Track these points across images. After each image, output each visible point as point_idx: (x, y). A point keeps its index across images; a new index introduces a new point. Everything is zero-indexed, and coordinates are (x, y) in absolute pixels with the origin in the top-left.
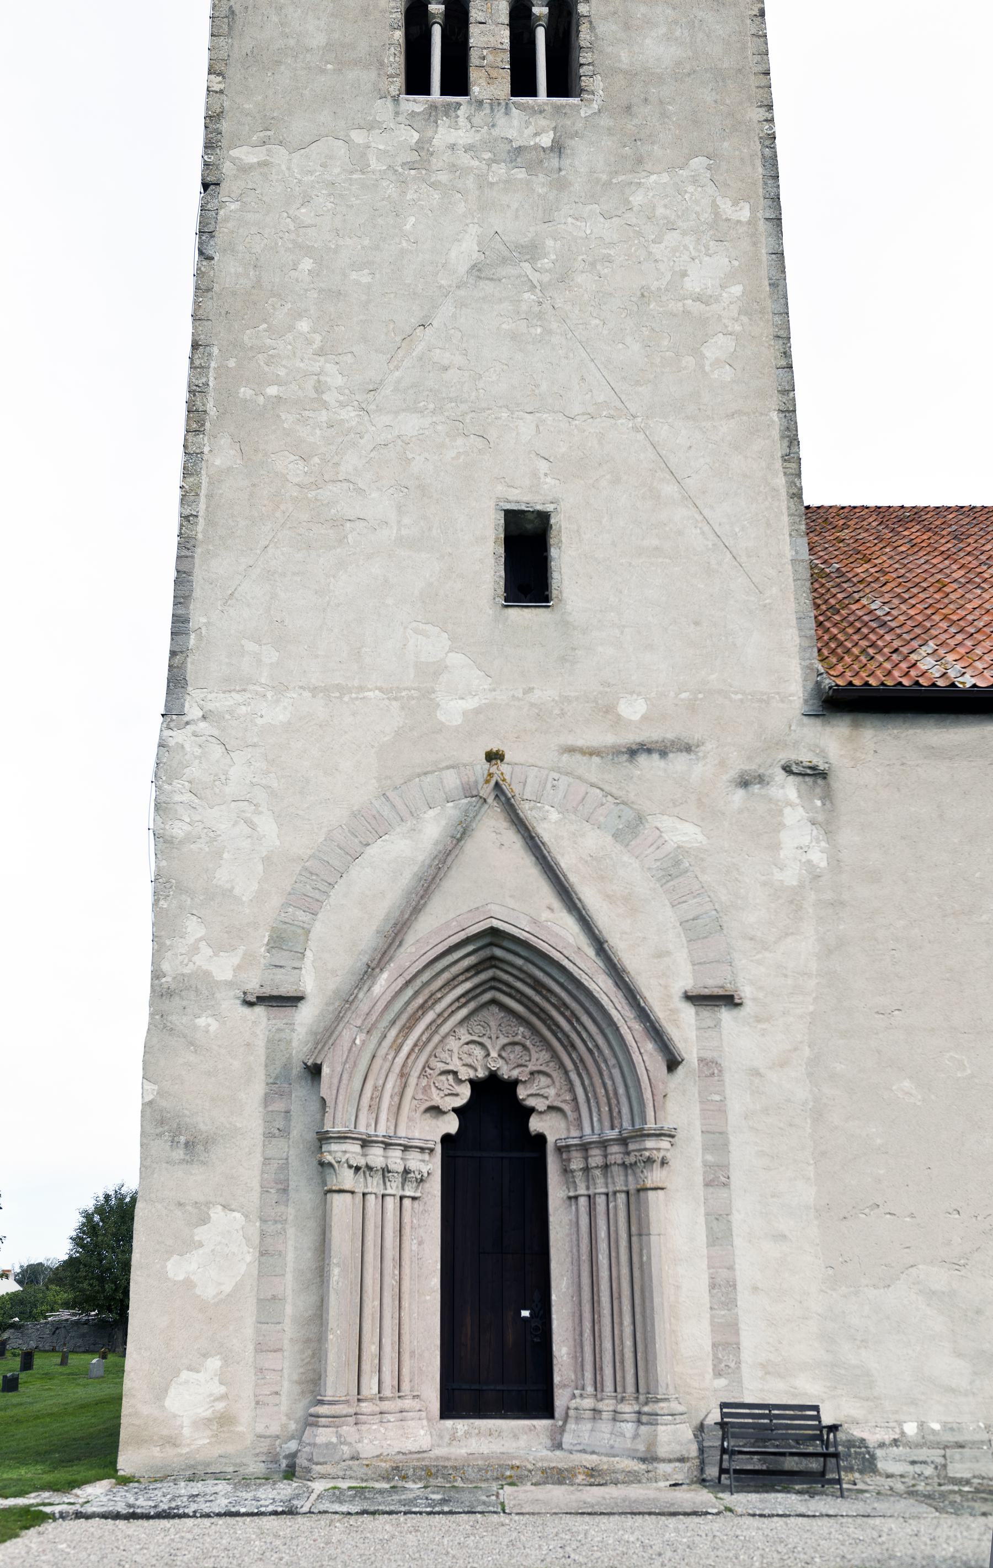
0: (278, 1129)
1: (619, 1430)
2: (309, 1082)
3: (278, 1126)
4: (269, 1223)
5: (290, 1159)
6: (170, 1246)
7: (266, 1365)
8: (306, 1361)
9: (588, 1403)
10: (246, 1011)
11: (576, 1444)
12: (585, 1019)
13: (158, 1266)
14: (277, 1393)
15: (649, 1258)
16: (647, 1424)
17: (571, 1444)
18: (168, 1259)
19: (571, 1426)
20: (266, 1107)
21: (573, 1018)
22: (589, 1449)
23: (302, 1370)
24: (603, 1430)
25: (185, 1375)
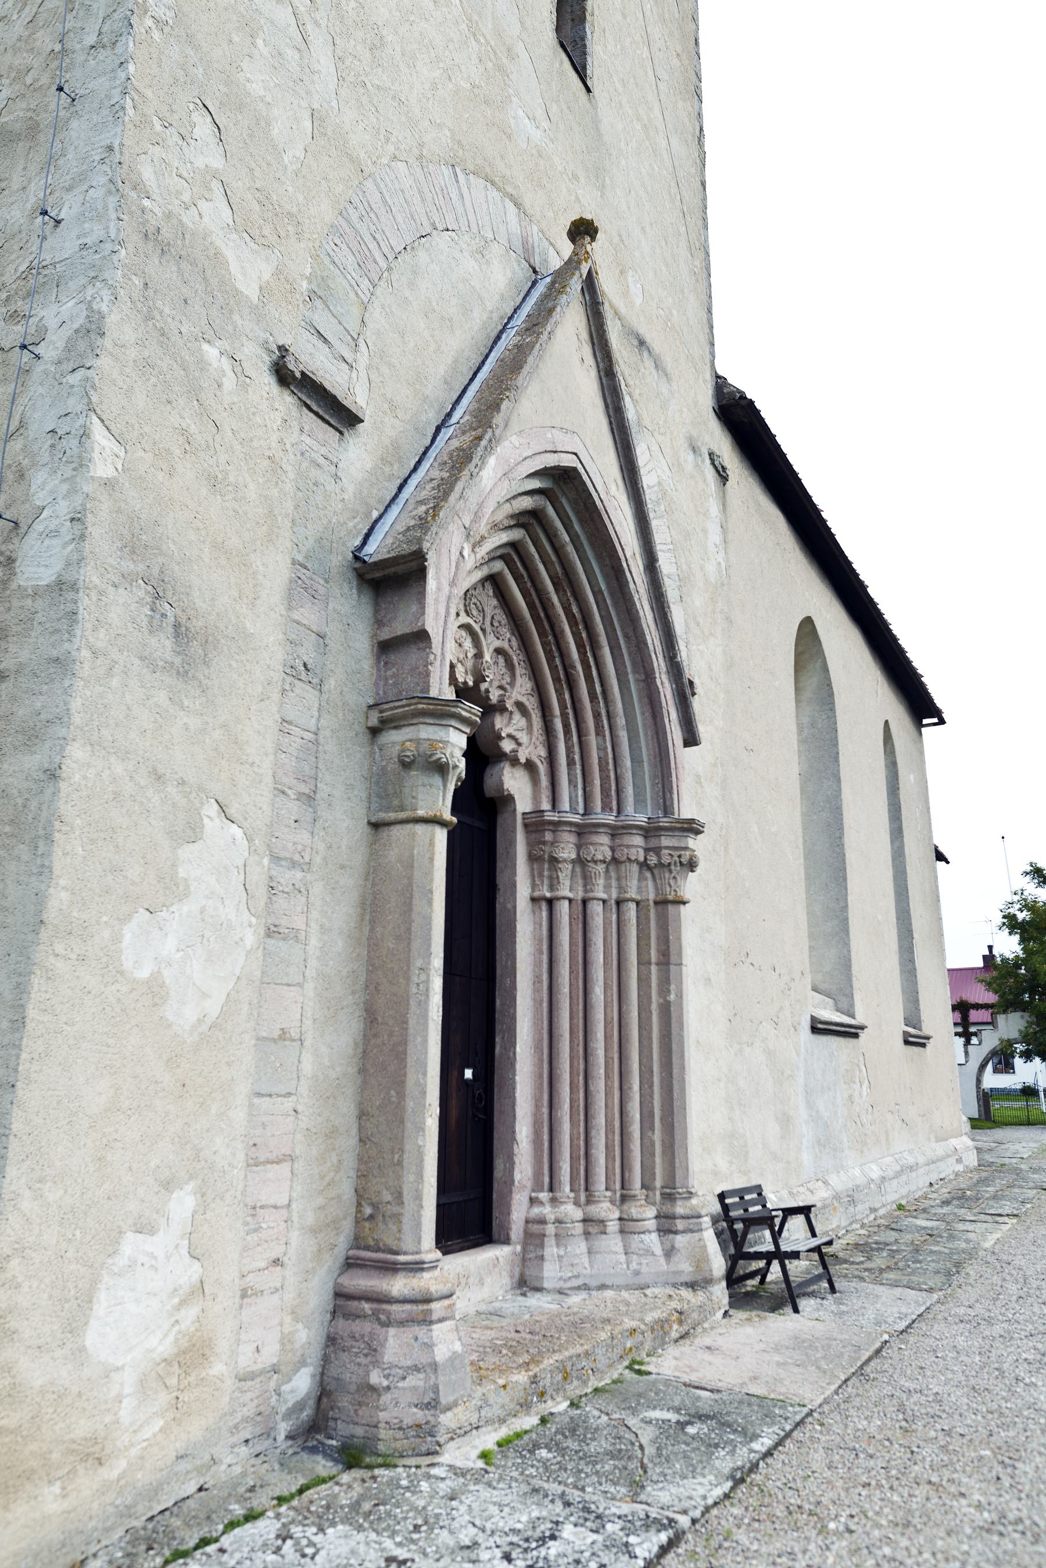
0: (305, 665)
1: (641, 1246)
2: (354, 591)
3: (305, 658)
4: (283, 863)
5: (321, 732)
6: (133, 883)
7: (264, 1199)
8: (327, 1179)
9: (572, 1212)
10: (268, 381)
11: (570, 1278)
12: (606, 652)
13: (106, 934)
14: (277, 1262)
15: (680, 996)
16: (683, 1232)
17: (561, 1279)
18: (127, 918)
19: (551, 1250)
20: (290, 608)
21: (589, 644)
22: (593, 1283)
23: (320, 1201)
24: (613, 1249)
25: (131, 1244)
